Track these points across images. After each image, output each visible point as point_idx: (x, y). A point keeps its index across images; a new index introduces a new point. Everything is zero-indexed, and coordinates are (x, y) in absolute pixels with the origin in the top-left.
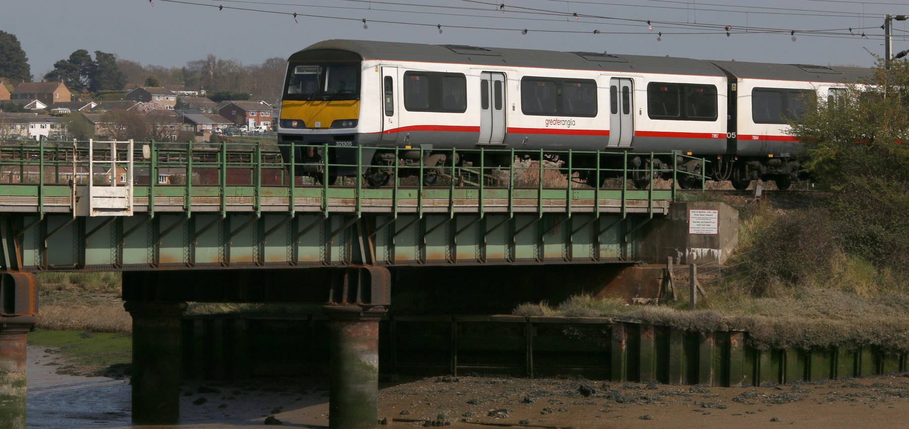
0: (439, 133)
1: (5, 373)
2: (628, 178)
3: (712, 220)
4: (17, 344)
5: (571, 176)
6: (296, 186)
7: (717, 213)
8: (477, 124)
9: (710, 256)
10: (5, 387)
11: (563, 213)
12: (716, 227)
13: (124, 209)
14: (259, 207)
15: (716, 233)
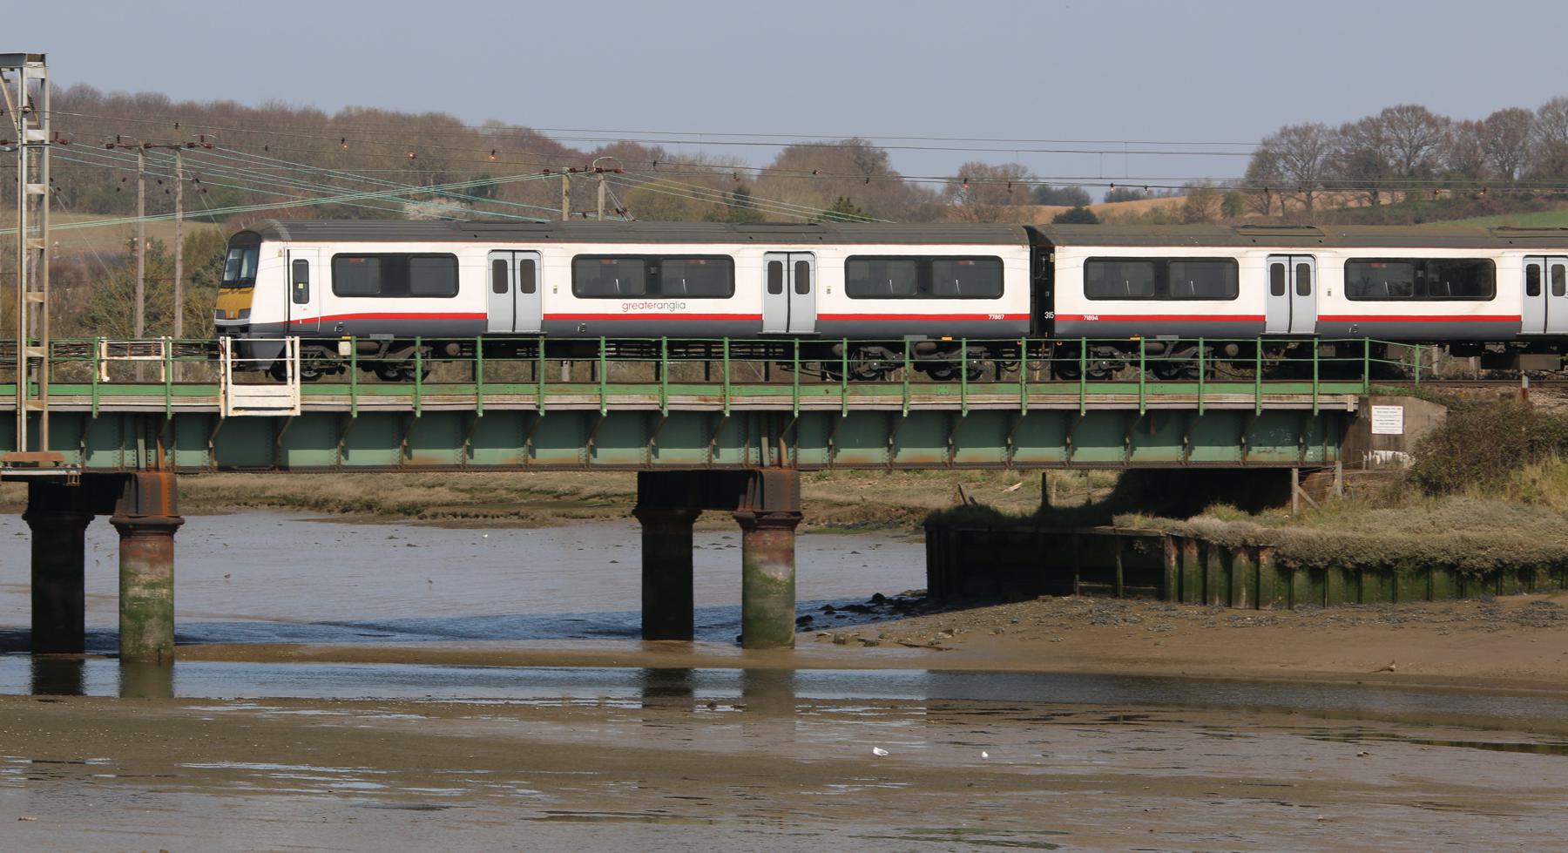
0: (1378, 323)
1: (136, 575)
2: (1147, 369)
3: (1397, 418)
4: (149, 546)
5: (666, 363)
6: (235, 381)
7: (1401, 411)
8: (483, 310)
9: (1396, 461)
10: (137, 589)
11: (1195, 410)
12: (1401, 425)
13: (292, 409)
14: (542, 405)
15: (1401, 432)
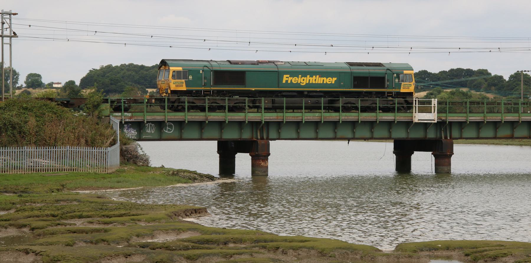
13: (434, 120)
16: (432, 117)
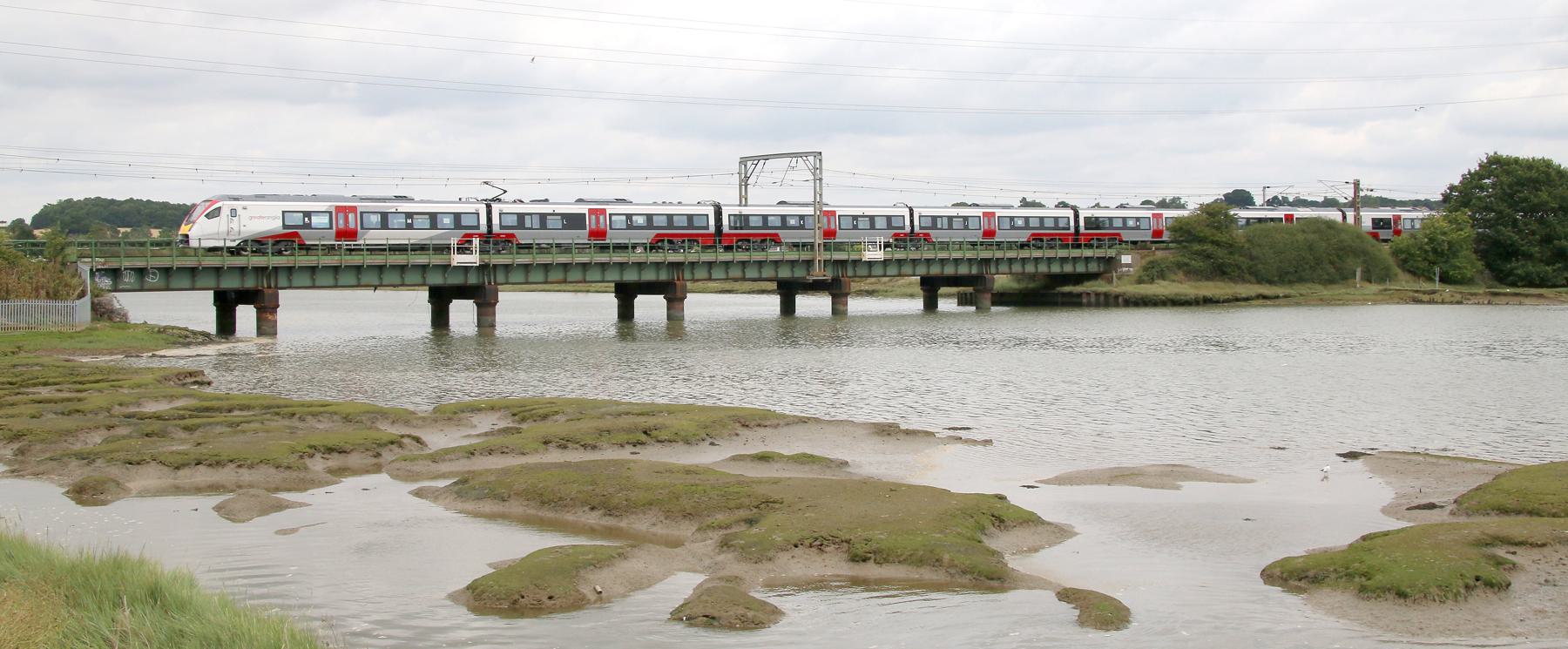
16: (473, 259)
